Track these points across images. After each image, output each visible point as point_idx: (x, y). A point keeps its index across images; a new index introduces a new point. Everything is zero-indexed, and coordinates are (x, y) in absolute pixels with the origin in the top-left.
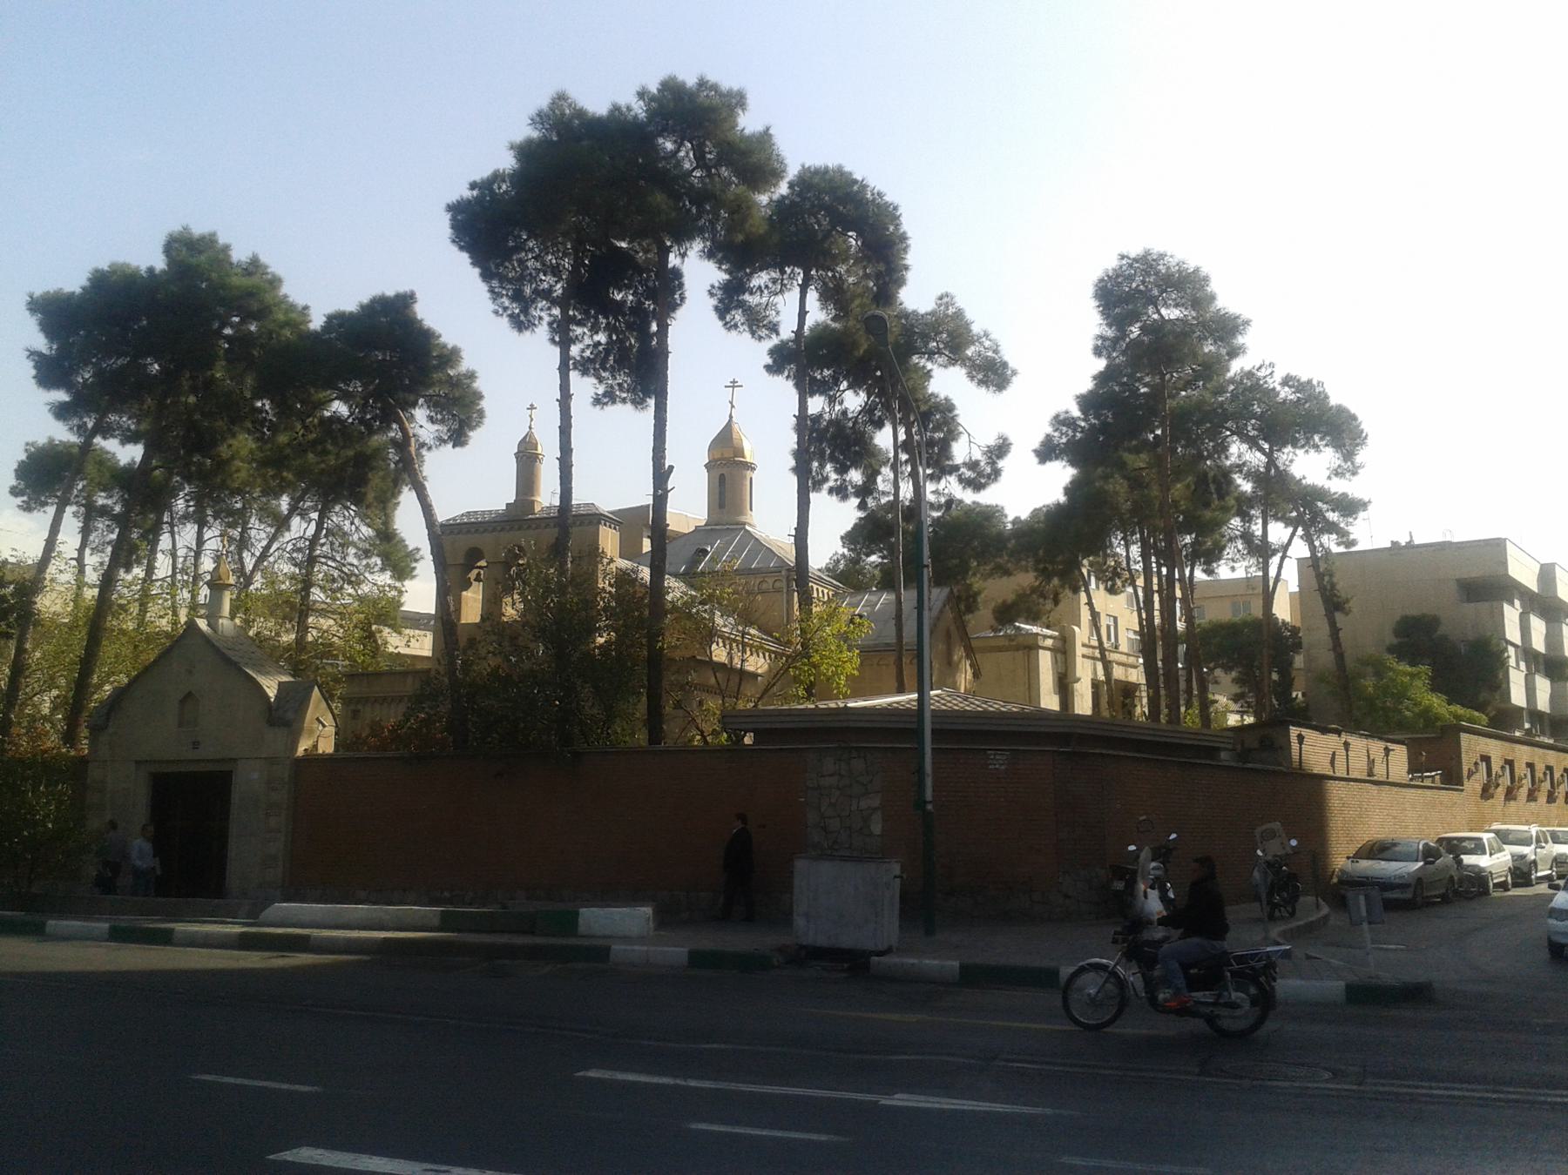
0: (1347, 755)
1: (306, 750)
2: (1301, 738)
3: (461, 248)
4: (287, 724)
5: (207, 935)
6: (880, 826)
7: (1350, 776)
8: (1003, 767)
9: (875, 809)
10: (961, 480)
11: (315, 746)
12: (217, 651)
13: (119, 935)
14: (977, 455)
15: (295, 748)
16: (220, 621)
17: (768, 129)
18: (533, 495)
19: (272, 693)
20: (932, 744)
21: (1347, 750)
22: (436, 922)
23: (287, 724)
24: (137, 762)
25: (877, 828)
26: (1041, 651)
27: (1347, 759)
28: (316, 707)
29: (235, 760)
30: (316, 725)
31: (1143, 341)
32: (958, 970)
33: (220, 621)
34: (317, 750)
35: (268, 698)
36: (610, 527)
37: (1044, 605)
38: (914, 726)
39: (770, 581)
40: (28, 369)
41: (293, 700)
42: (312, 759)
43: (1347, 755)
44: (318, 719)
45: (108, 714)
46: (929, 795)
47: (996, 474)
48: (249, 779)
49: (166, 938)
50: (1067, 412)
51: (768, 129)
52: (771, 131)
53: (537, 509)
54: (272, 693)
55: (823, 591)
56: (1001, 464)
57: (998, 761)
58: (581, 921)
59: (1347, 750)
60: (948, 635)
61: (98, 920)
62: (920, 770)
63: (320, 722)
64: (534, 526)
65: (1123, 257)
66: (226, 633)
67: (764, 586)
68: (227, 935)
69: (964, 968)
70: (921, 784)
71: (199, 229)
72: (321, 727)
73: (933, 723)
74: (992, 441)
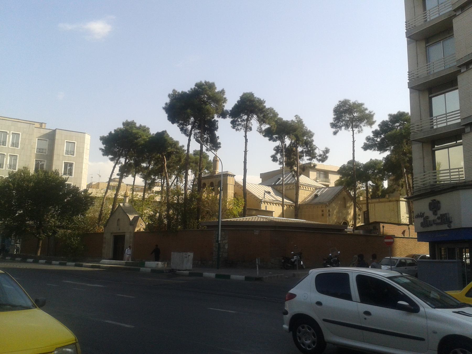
0: (409, 231)
1: (137, 230)
2: (383, 227)
3: (170, 121)
4: (133, 225)
5: (87, 265)
6: (227, 246)
7: (410, 237)
8: (258, 234)
9: (226, 243)
10: (317, 160)
11: (140, 230)
12: (122, 209)
13: (76, 265)
14: (322, 153)
15: (134, 230)
16: (125, 204)
17: (223, 89)
18: (216, 170)
19: (131, 219)
20: (221, 228)
21: (409, 230)
22: (125, 264)
23: (133, 225)
24: (111, 233)
25: (226, 247)
26: (401, 202)
27: (409, 233)
28: (140, 221)
29: (125, 232)
30: (140, 225)
31: (131, 163)
32: (244, 278)
33: (125, 204)
34: (140, 230)
35: (130, 219)
36: (231, 176)
37: (399, 188)
38: (217, 224)
39: (292, 186)
40: (101, 153)
41: (136, 219)
42: (139, 232)
43: (409, 231)
44: (141, 224)
45: (107, 223)
46: (219, 239)
47: (326, 157)
48: (127, 236)
49: (81, 266)
50: (369, 136)
51: (223, 89)
52: (224, 90)
53: (217, 173)
54: (131, 219)
55: (313, 189)
56: (327, 155)
57: (257, 232)
58: (145, 264)
59: (409, 230)
60: (344, 198)
61: (73, 263)
62: (218, 234)
63: (141, 224)
64: (215, 177)
65: (340, 102)
66: (126, 206)
67: (290, 188)
68: (90, 265)
69: (189, 273)
70: (218, 237)
71: (130, 120)
72: (141, 225)
73: (221, 224)
74: (324, 149)
